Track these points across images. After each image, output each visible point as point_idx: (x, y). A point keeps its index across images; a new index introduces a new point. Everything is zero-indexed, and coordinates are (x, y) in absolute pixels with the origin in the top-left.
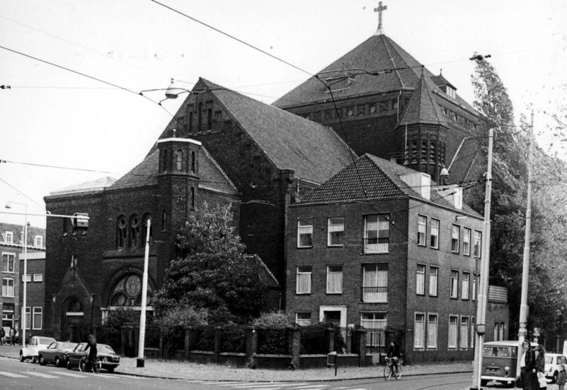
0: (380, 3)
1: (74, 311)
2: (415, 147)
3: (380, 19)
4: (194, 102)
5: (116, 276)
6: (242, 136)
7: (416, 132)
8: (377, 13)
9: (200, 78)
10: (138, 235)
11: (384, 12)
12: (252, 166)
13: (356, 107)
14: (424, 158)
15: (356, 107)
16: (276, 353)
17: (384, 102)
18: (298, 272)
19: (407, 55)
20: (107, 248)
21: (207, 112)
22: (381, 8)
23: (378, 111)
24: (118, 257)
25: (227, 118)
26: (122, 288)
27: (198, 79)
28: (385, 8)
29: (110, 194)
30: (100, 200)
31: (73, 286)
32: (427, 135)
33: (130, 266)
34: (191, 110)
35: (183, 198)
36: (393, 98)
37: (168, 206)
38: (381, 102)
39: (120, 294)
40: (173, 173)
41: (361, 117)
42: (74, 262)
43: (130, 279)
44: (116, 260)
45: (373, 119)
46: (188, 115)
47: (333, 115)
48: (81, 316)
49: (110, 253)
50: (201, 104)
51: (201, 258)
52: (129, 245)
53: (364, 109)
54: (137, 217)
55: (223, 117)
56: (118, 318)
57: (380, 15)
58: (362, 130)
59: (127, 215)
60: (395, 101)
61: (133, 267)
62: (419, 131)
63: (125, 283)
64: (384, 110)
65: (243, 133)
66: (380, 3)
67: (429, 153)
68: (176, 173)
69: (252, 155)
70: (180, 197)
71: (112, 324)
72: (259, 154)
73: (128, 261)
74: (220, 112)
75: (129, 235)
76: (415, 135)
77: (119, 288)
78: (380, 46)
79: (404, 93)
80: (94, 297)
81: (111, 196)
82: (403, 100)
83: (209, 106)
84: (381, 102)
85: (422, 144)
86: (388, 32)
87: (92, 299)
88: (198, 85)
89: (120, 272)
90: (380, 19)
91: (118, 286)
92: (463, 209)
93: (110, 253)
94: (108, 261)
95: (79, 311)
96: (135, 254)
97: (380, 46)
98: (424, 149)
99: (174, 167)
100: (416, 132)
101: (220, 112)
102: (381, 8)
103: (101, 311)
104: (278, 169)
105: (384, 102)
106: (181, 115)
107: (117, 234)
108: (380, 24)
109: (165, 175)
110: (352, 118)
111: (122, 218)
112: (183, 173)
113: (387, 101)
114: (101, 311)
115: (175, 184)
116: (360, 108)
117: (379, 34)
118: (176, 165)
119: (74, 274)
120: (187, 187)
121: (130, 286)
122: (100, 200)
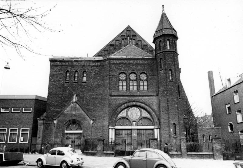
16: (110, 151)
27: (127, 26)
31: (74, 113)
42: (76, 98)
44: (122, 97)
61: (137, 102)
63: (127, 112)
74: (141, 41)
91: (121, 113)
94: (115, 97)
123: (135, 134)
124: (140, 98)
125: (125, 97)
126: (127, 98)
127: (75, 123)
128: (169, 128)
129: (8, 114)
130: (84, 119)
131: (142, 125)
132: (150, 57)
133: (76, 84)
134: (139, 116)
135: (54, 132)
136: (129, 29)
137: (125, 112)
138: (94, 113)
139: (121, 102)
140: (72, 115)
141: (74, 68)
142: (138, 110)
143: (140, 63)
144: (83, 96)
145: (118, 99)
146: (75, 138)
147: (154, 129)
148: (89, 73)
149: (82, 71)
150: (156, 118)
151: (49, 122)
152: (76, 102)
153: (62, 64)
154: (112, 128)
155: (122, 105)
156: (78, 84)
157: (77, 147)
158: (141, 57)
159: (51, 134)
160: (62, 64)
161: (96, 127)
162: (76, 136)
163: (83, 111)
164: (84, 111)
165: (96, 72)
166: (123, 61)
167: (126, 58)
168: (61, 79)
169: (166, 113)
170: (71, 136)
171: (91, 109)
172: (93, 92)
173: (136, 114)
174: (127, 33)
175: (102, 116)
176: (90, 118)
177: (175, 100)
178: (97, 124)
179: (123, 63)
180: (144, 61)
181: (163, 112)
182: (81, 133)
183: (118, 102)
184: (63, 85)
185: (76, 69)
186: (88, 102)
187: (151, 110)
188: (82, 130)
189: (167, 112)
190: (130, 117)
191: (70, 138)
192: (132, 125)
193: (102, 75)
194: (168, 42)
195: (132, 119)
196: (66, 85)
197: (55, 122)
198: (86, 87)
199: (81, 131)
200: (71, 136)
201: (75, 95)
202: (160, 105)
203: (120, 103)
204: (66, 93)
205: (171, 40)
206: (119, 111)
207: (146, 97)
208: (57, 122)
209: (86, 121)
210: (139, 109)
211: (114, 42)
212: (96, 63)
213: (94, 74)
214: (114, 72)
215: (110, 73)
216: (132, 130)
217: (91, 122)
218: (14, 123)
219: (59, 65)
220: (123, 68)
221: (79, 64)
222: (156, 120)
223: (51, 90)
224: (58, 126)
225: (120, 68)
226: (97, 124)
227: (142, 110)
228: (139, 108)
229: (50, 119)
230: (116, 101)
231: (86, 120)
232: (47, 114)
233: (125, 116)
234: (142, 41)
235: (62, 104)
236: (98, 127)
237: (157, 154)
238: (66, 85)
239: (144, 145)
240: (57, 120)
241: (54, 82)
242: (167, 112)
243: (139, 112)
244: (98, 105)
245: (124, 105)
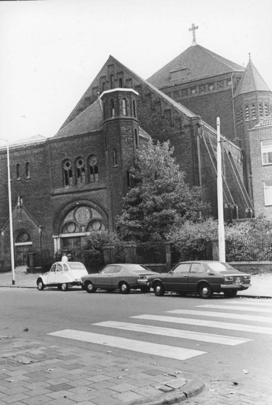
0: (193, 25)
1: (21, 242)
2: (253, 108)
3: (194, 36)
4: (106, 74)
5: (67, 208)
6: (152, 95)
7: (254, 97)
8: (192, 31)
9: (110, 56)
10: (83, 174)
11: (196, 31)
12: (163, 117)
13: (198, 88)
14: (261, 115)
15: (198, 88)
16: (161, 263)
17: (219, 82)
18: (265, 187)
19: (220, 57)
20: (54, 186)
21: (118, 81)
22: (194, 28)
23: (198, 92)
24: (67, 193)
25: (138, 83)
26: (72, 218)
27: (108, 57)
28: (197, 27)
29: (54, 142)
30: (42, 149)
31: (20, 221)
32: (262, 99)
33: (79, 199)
34: (103, 80)
35: (130, 138)
36: (228, 77)
37: (119, 145)
38: (217, 82)
39: (70, 223)
40: (121, 117)
41: (203, 93)
42: (20, 202)
43: (78, 210)
44: (65, 195)
45: (212, 94)
46: (102, 85)
47: (181, 95)
48: (31, 245)
49: (57, 191)
50: (112, 75)
51: (159, 184)
52: (76, 183)
53: (205, 88)
54: (82, 160)
55: (133, 82)
56: (98, 240)
57: (194, 33)
58: (204, 103)
59: (72, 158)
60: (229, 80)
61: (82, 199)
62: (257, 97)
63: (74, 214)
64: (220, 87)
65: (153, 93)
66: (193, 25)
67: (251, 112)
68: (123, 117)
69: (162, 109)
70: (128, 137)
71: (94, 246)
72: (169, 108)
73: (76, 195)
74: (130, 80)
75: (75, 174)
76: (253, 99)
77: (67, 220)
78: (197, 52)
79: (235, 73)
80: (41, 228)
81: (55, 144)
82: (235, 79)
83: (120, 76)
84: (217, 82)
85: (259, 106)
86: (199, 43)
87: (40, 230)
88: (108, 61)
89: (70, 205)
90: (194, 36)
91: (67, 216)
92: (264, 154)
93: (57, 191)
94: (57, 197)
95: (27, 241)
96: (83, 189)
97: (197, 52)
98: (261, 109)
99: (121, 112)
100: (254, 97)
101: (130, 80)
102: (194, 28)
103: (53, 238)
104: (188, 117)
105: (219, 82)
106: (95, 86)
107: (63, 175)
108: (194, 39)
109: (113, 120)
110: (196, 95)
111: (66, 162)
112: (128, 117)
113: (223, 81)
114: (53, 238)
115: (123, 126)
116: (201, 87)
117: (194, 45)
118: (122, 111)
119: (21, 211)
120: (132, 128)
121: (79, 216)
122: (42, 149)
124: (86, 193)
125: (69, 195)
130: (32, 227)
132: (98, 130)
134: (88, 219)
135: (3, 246)
137: (72, 215)
138: (42, 218)
139: (65, 202)
143: (87, 141)
145: (59, 199)
152: (21, 206)
154: (55, 236)
155: (65, 207)
158: (87, 132)
161: (46, 237)
165: (41, 162)
171: (39, 214)
174: (108, 71)
177: (120, 193)
178: (46, 232)
179: (65, 145)
180: (91, 137)
183: (61, 202)
187: (100, 209)
190: (78, 221)
191: (21, 252)
194: (124, 101)
195: (80, 222)
198: (30, 184)
199: (30, 243)
200: (21, 250)
201: (19, 198)
205: (116, 99)
206: (63, 214)
207: (94, 192)
212: (39, 149)
214: (57, 160)
220: (67, 152)
225: (63, 152)
227: (92, 209)
231: (34, 229)
234: (133, 79)
237: (180, 265)
244: (46, 207)
245: (67, 207)
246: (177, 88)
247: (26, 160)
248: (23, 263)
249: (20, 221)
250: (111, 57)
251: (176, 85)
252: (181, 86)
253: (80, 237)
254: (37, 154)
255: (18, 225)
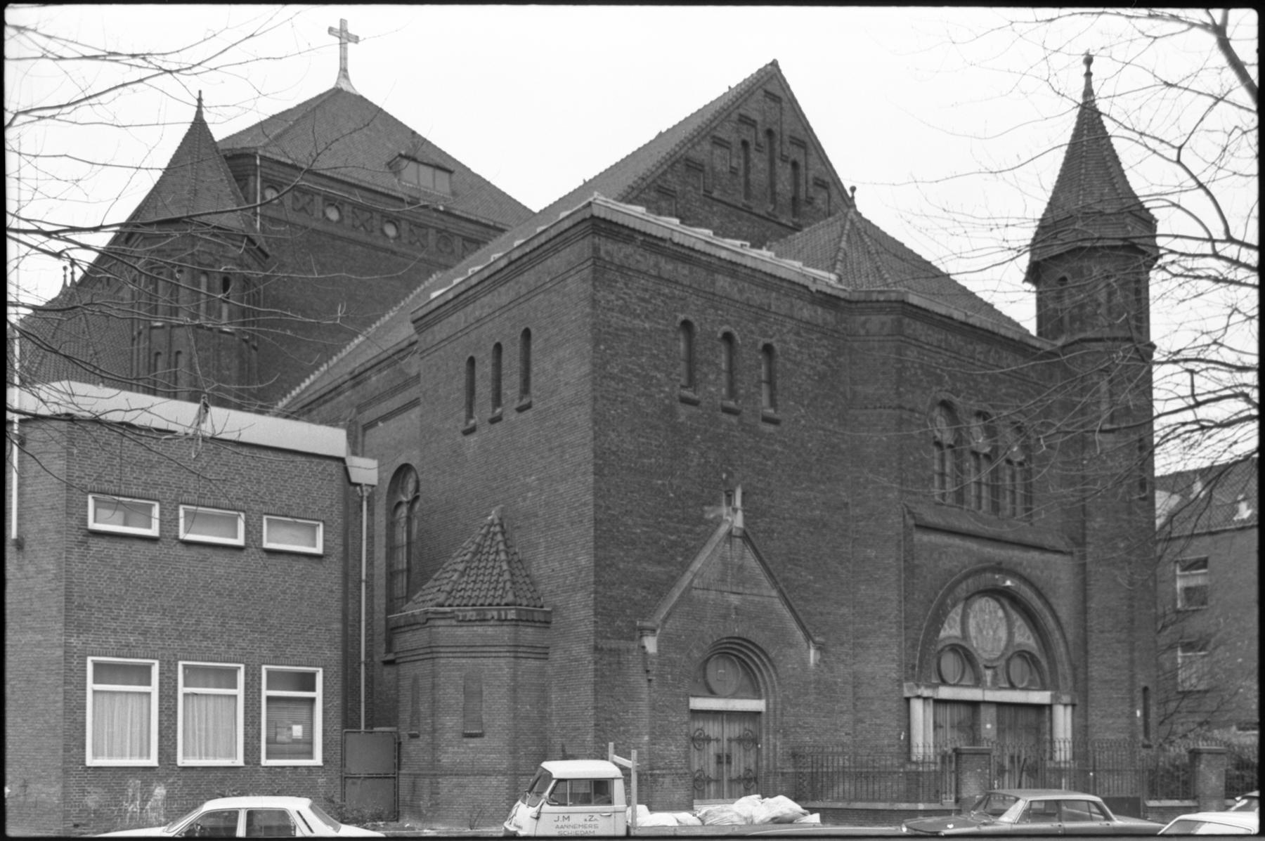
0: (331, 30)
31: (735, 600)
44: (957, 541)
66: (356, 40)
80: (821, 648)
123: (989, 726)
126: (973, 545)
127: (742, 656)
128: (1133, 706)
129: (154, 549)
131: (1007, 685)
133: (734, 420)
135: (644, 707)
136: (773, 88)
140: (728, 608)
141: (716, 309)
142: (1001, 613)
144: (766, 501)
146: (730, 740)
147: (1050, 706)
148: (789, 366)
149: (755, 344)
150: (1064, 658)
151: (613, 644)
153: (656, 265)
156: (740, 422)
157: (742, 787)
159: (630, 715)
160: (656, 265)
162: (735, 730)
163: (774, 593)
164: (780, 591)
166: (662, 262)
167: (962, 323)
168: (657, 368)
169: (1119, 642)
170: (712, 729)
172: (812, 490)
173: (995, 632)
175: (850, 628)
176: (808, 637)
181: (1102, 632)
182: (759, 713)
184: (670, 411)
185: (728, 322)
186: (793, 542)
188: (760, 698)
189: (1123, 636)
191: (708, 739)
192: (978, 682)
193: (841, 389)
196: (683, 412)
197: (651, 644)
198: (778, 447)
202: (1085, 599)
203: (951, 573)
204: (688, 467)
208: (659, 642)
209: (792, 651)
210: (1003, 607)
211: (707, 146)
213: (808, 377)
215: (899, 394)
216: (982, 708)
217: (813, 656)
218: (209, 624)
219: (643, 267)
221: (741, 291)
222: (1064, 668)
223: (613, 435)
224: (667, 669)
226: (831, 670)
228: (1006, 603)
229: (618, 623)
230: (936, 556)
231: (791, 645)
232: (600, 589)
233: (956, 637)
235: (673, 538)
236: (836, 683)
238: (682, 419)
239: (1010, 772)
240: (658, 631)
241: (622, 380)
242: (1123, 636)
243: (1004, 621)
245: (964, 585)
246: (451, 225)
247: (765, 334)
248: (713, 787)
249: (735, 600)
250: (774, 64)
251: (447, 213)
252: (463, 224)
253: (974, 705)
254: (810, 326)
255: (725, 617)
